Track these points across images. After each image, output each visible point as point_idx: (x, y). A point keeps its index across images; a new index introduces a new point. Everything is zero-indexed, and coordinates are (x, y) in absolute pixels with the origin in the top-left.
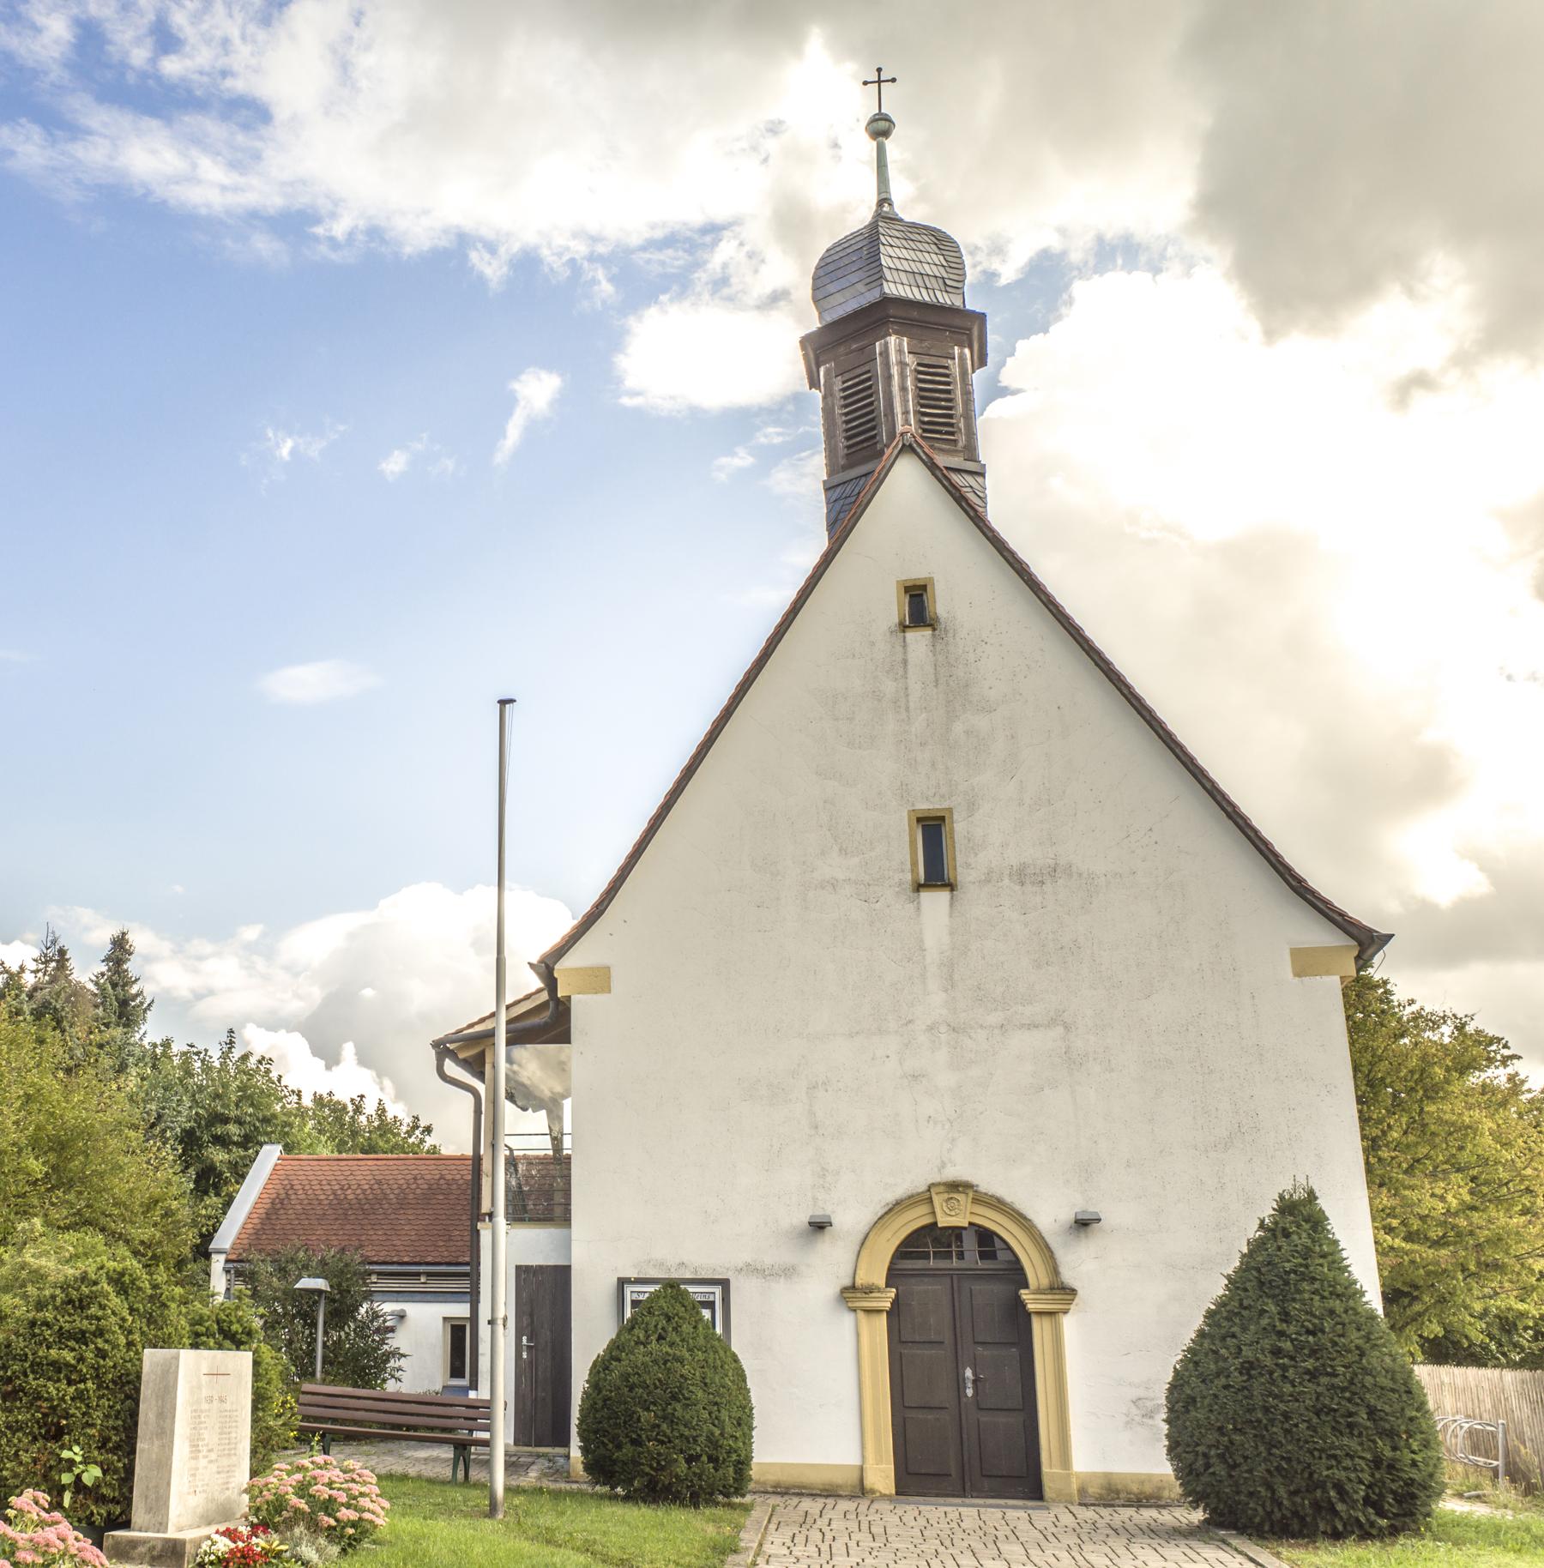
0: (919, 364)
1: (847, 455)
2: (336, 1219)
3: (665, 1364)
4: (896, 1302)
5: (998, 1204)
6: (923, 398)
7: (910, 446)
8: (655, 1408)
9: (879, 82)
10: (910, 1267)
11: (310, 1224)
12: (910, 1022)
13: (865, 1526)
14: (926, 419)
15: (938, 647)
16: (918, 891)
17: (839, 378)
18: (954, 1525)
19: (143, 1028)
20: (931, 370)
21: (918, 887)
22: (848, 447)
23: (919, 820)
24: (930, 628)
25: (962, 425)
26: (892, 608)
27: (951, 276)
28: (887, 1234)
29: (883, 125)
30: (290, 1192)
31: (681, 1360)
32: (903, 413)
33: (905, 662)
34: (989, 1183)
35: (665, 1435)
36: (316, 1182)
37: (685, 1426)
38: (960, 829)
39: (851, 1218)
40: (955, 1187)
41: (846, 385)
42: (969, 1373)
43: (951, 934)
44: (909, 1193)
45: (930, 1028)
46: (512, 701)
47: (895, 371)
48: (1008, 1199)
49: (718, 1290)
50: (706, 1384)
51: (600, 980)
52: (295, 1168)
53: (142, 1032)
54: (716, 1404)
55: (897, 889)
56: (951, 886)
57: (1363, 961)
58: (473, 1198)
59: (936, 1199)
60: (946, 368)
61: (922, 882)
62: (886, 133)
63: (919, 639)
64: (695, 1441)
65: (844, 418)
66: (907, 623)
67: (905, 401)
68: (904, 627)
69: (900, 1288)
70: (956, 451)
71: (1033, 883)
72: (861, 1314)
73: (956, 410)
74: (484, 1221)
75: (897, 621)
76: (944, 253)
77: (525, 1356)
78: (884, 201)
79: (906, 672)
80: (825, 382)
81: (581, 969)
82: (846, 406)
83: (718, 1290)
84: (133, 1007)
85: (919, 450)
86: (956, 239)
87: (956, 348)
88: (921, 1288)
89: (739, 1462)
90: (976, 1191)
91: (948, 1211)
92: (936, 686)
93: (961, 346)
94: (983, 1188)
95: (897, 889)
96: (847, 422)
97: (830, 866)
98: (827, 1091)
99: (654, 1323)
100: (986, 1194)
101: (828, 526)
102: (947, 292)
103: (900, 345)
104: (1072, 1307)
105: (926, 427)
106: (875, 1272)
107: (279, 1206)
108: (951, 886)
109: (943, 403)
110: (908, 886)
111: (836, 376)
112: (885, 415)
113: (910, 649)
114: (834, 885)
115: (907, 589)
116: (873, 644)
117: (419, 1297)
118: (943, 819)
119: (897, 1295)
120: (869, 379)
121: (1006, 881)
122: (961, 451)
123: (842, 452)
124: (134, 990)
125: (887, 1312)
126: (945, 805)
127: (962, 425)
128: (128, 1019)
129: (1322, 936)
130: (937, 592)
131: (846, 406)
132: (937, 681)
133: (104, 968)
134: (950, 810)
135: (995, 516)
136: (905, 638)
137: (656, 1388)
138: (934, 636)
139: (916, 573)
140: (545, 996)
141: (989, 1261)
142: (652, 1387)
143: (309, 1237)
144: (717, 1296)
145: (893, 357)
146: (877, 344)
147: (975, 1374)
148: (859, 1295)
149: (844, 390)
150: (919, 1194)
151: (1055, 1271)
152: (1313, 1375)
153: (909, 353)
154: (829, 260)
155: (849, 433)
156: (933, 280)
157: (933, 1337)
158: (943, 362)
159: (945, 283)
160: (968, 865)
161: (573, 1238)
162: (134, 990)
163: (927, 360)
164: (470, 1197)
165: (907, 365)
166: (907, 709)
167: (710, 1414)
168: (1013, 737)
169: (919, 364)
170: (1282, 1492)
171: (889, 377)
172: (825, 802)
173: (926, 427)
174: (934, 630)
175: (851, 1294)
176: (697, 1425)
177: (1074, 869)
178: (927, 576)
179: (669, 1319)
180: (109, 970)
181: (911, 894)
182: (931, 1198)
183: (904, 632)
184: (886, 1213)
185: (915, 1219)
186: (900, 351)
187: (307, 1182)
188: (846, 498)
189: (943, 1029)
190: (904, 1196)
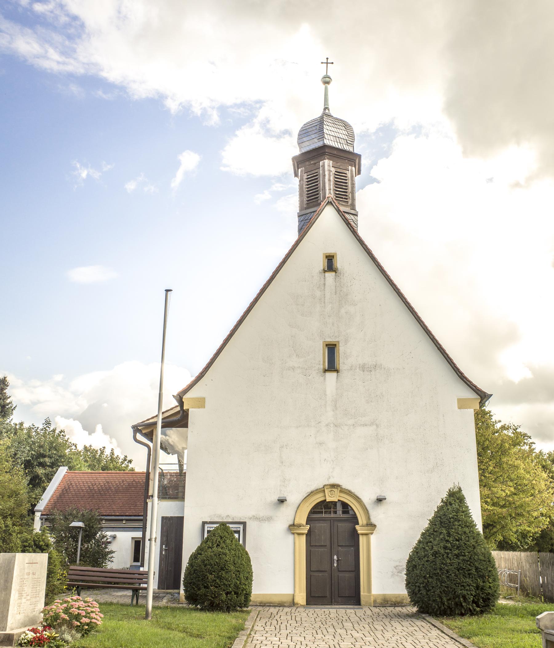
1: (307, 204)
4: (309, 531)
5: (349, 493)
7: (331, 202)
9: (327, 63)
10: (317, 517)
13: (293, 618)
14: (337, 192)
15: (337, 279)
18: (327, 616)
19: (11, 417)
21: (325, 371)
23: (327, 345)
24: (334, 272)
25: (350, 196)
26: (321, 263)
28: (307, 504)
29: (327, 79)
30: (70, 486)
31: (225, 554)
32: (329, 190)
33: (325, 284)
34: (346, 485)
38: (341, 350)
40: (333, 486)
41: (308, 177)
42: (335, 557)
43: (337, 389)
44: (316, 488)
45: (327, 425)
49: (241, 526)
50: (235, 564)
51: (201, 403)
53: (11, 419)
54: (238, 571)
55: (317, 371)
56: (337, 371)
57: (482, 404)
59: (326, 491)
62: (328, 83)
63: (330, 276)
64: (230, 586)
65: (307, 190)
67: (330, 185)
68: (325, 271)
69: (311, 525)
70: (347, 206)
71: (367, 371)
72: (296, 535)
76: (347, 130)
77: (164, 553)
79: (325, 288)
80: (301, 175)
82: (308, 185)
83: (241, 526)
84: (7, 408)
85: (334, 204)
86: (352, 125)
88: (318, 525)
89: (246, 594)
90: (341, 488)
93: (352, 166)
94: (344, 487)
95: (317, 371)
100: (345, 489)
101: (298, 230)
105: (337, 195)
108: (337, 371)
109: (344, 187)
110: (321, 370)
111: (305, 173)
112: (322, 190)
114: (293, 368)
115: (327, 257)
116: (313, 277)
117: (122, 529)
118: (335, 345)
120: (317, 175)
121: (358, 370)
123: (305, 202)
124: (8, 401)
126: (337, 340)
127: (350, 196)
128: (5, 413)
129: (469, 394)
130: (338, 259)
131: (308, 185)
134: (338, 342)
135: (361, 232)
137: (215, 565)
138: (336, 275)
139: (330, 251)
140: (178, 409)
146: (321, 162)
147: (338, 558)
148: (296, 528)
149: (307, 179)
150: (320, 489)
151: (369, 518)
152: (457, 556)
154: (305, 128)
155: (308, 195)
157: (323, 544)
158: (345, 171)
160: (344, 363)
162: (8, 401)
163: (339, 170)
167: (236, 575)
168: (363, 315)
169: (336, 172)
170: (445, 599)
171: (324, 175)
173: (337, 195)
174: (336, 273)
177: (383, 366)
179: (221, 538)
182: (324, 490)
184: (307, 496)
185: (319, 498)
188: (306, 220)
189: (332, 425)
190: (315, 489)
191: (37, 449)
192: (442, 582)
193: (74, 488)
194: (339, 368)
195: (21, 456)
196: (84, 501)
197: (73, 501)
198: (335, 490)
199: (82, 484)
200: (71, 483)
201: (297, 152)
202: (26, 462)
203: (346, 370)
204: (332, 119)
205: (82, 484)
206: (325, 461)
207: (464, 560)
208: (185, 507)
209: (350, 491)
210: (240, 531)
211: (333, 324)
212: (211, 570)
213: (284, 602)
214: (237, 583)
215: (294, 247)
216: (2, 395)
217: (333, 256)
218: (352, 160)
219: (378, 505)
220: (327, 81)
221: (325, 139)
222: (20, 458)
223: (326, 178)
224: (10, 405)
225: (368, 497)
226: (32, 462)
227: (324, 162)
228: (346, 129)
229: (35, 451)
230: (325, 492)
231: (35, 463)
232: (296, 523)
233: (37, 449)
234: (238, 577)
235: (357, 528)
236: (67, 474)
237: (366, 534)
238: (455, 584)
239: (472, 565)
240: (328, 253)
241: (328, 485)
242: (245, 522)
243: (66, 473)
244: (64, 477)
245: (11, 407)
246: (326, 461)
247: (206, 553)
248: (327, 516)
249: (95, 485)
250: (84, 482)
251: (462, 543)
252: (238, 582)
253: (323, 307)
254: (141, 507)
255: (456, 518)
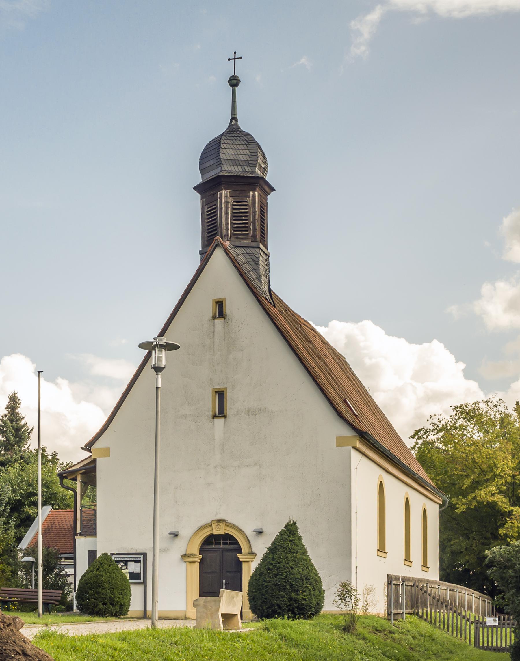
0: (234, 202)
2: (70, 536)
3: (97, 577)
4: (202, 559)
5: (233, 526)
6: (234, 216)
8: (93, 590)
9: (235, 59)
10: (208, 548)
11: (59, 538)
12: (209, 465)
14: (235, 226)
15: (226, 326)
16: (214, 418)
17: (206, 206)
19: (29, 442)
20: (239, 204)
21: (215, 416)
22: (208, 237)
23: (216, 392)
24: (223, 318)
25: (251, 227)
26: (210, 310)
27: (252, 159)
28: (198, 537)
29: (234, 82)
30: (53, 526)
31: (102, 576)
32: (226, 224)
33: (214, 332)
34: (231, 520)
35: (96, 597)
36: (64, 521)
37: (102, 594)
38: (229, 395)
39: (186, 532)
40: (219, 521)
42: (224, 581)
43: (224, 433)
44: (206, 523)
45: (215, 467)
46: (42, 372)
47: (223, 206)
48: (237, 525)
49: (142, 557)
50: (110, 583)
51: (106, 452)
52: (56, 515)
53: (28, 444)
54: (113, 588)
55: (207, 418)
56: (225, 417)
58: (74, 528)
59: (213, 525)
60: (246, 202)
61: (217, 415)
62: (236, 85)
63: (219, 322)
64: (106, 599)
65: (207, 224)
66: (217, 316)
67: (227, 219)
68: (214, 318)
69: (204, 555)
70: (248, 238)
71: (252, 415)
72: (188, 563)
73: (249, 221)
74: (78, 536)
75: (212, 315)
78: (234, 118)
79: (214, 336)
81: (100, 448)
82: (208, 219)
84: (22, 432)
87: (251, 192)
88: (209, 554)
89: (121, 605)
90: (227, 522)
91: (217, 529)
92: (224, 341)
94: (229, 522)
95: (207, 418)
96: (208, 226)
97: (185, 410)
98: (180, 489)
99: (96, 565)
100: (230, 523)
102: (249, 166)
103: (227, 194)
104: (254, 560)
105: (235, 229)
106: (195, 549)
107: (48, 531)
108: (225, 417)
109: (244, 218)
110: (211, 417)
111: (205, 205)
113: (216, 326)
114: (185, 416)
115: (217, 303)
116: (203, 325)
119: (202, 557)
121: (244, 414)
122: (250, 238)
123: (206, 239)
124: (23, 422)
125: (199, 563)
126: (225, 387)
127: (251, 227)
128: (20, 438)
130: (227, 304)
131: (208, 219)
132: (224, 339)
133: (6, 412)
134: (226, 388)
136: (214, 322)
137: (94, 583)
138: (224, 321)
141: (232, 545)
142: (93, 583)
143: (58, 544)
144: (142, 558)
145: (223, 200)
146: (218, 193)
147: (226, 582)
148: (186, 557)
150: (208, 524)
151: (250, 547)
152: (276, 575)
153: (230, 197)
155: (209, 231)
156: (244, 162)
157: (213, 570)
158: (245, 199)
159: (249, 163)
160: (231, 409)
161: (97, 541)
162: (23, 422)
163: (238, 199)
164: (73, 527)
165: (228, 202)
166: (214, 350)
167: (111, 591)
168: (249, 360)
169: (234, 202)
170: (264, 608)
171: (221, 209)
172: (184, 386)
173: (235, 229)
174: (225, 319)
175: (185, 557)
176: (106, 594)
177: (267, 410)
178: (224, 297)
179: (101, 564)
180: (9, 413)
181: (211, 420)
182: (212, 525)
183: (214, 320)
184: (198, 530)
185: (207, 533)
186: (226, 197)
187: (60, 521)
189: (219, 467)
190: (204, 524)
191: (25, 487)
192: (263, 595)
193: (56, 527)
194: (227, 413)
195: (4, 497)
196: (64, 539)
197: (55, 540)
198: (221, 524)
199: (65, 523)
200: (54, 523)
201: (199, 179)
202: (16, 501)
203: (233, 415)
204: (233, 138)
205: (65, 523)
206: (213, 499)
207: (281, 578)
208: (97, 542)
209: (234, 525)
210: (140, 560)
211: (221, 371)
212: (91, 588)
213: (179, 617)
214: (111, 597)
215: (184, 297)
216: (14, 416)
217: (222, 302)
218: (254, 183)
219: (258, 537)
220: (234, 82)
221: (222, 165)
222: (4, 499)
223: (223, 211)
224: (25, 427)
225: (249, 531)
226: (23, 501)
227: (221, 193)
228: (247, 147)
229: (23, 490)
230: (212, 526)
231: (26, 503)
232: (188, 553)
233: (25, 487)
234: (113, 592)
235: (238, 556)
236: (50, 513)
237: (248, 562)
238: (271, 596)
239: (287, 582)
240: (218, 299)
241: (215, 520)
242: (146, 554)
243: (50, 512)
244: (47, 516)
245: (28, 430)
246: (214, 500)
247: (88, 575)
248: (217, 546)
249: (54, 524)
250: (66, 520)
251: (281, 565)
252: (113, 596)
253: (212, 354)
254: (71, 541)
255: (282, 546)
